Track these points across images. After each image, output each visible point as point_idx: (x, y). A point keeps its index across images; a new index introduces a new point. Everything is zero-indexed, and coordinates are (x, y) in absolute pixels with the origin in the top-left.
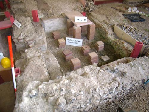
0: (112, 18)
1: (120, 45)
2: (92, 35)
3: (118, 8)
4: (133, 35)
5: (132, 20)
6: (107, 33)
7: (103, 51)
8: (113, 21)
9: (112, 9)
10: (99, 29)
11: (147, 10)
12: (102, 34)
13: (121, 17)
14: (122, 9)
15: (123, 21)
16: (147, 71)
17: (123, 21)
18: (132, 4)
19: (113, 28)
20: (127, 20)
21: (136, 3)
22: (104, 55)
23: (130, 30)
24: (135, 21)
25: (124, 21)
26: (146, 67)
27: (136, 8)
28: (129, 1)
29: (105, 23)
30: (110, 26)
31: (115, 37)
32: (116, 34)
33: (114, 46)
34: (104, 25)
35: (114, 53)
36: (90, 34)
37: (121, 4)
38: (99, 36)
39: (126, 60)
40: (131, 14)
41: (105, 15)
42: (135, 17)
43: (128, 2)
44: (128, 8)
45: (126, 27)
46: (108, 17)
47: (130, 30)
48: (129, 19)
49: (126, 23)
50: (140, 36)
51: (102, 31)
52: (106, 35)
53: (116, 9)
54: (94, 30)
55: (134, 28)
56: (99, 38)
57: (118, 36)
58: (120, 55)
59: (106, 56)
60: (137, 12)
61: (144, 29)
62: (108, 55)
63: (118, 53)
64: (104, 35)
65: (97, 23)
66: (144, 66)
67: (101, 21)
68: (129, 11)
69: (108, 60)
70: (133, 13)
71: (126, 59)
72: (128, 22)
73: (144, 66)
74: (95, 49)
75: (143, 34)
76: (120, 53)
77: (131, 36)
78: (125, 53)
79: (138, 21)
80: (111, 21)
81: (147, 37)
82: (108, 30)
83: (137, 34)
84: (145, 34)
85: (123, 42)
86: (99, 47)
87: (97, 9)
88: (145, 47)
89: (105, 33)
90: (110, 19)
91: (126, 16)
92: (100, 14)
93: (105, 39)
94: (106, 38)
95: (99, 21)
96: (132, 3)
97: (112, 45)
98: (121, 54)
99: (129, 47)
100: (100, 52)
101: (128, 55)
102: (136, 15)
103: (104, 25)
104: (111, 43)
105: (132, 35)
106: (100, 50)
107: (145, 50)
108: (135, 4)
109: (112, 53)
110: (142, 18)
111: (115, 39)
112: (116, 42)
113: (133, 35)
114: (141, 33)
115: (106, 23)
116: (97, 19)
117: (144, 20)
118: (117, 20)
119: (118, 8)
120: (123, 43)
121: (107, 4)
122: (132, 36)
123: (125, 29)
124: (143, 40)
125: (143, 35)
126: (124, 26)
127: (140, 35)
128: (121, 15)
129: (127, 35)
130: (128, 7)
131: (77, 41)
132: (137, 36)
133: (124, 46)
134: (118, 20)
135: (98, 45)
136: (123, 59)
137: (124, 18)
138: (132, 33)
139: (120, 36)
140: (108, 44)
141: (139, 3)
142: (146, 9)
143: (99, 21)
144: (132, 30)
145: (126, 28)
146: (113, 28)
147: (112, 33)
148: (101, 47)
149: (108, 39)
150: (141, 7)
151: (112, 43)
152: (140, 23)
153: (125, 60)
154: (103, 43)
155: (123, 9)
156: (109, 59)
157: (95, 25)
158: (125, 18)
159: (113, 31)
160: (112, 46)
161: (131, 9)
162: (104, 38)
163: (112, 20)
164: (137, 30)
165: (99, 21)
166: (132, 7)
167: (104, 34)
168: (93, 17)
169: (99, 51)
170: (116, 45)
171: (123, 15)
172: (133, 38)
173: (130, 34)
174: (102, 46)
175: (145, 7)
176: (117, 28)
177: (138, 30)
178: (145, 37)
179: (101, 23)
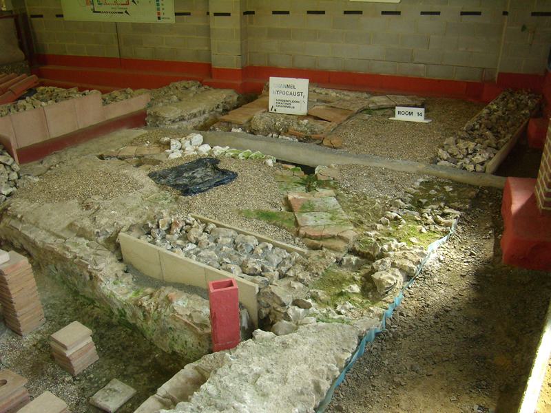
0: (107, 203)
1: (159, 313)
2: (26, 309)
3: (131, 151)
4: (202, 253)
5: (186, 191)
6: (96, 278)
7: (97, 366)
8: (112, 216)
9: (104, 165)
10: (59, 267)
11: (236, 134)
12: (80, 287)
13: (142, 186)
14: (146, 152)
15: (154, 202)
16: (279, 398)
17: (154, 202)
18: (184, 123)
19: (113, 244)
20: (170, 194)
21: (195, 116)
22: (108, 381)
23: (185, 238)
24: (200, 191)
25: (157, 204)
26: (271, 380)
27: (198, 138)
28: (166, 115)
29: (80, 236)
30: (101, 239)
31: (136, 282)
32: (138, 266)
33: (139, 324)
34: (76, 245)
35: (150, 352)
36: (16, 306)
37: (142, 132)
38: (71, 298)
39: (196, 372)
40: (181, 163)
41: (74, 197)
42: (199, 174)
43: (164, 118)
44: (168, 144)
45: (166, 228)
46: (89, 200)
47: (185, 238)
48: (176, 186)
49: (167, 209)
50: (228, 245)
51: (72, 273)
52: (93, 287)
53: (122, 159)
54: (31, 281)
55: (202, 221)
56: (70, 310)
57: (147, 273)
58: (174, 353)
59: (117, 385)
60: (205, 149)
61: (240, 212)
62: (124, 377)
63: (167, 350)
64: (88, 290)
65: (44, 243)
66: (264, 381)
67: (56, 230)
68: (175, 153)
69: (129, 400)
70: (188, 156)
71: (196, 368)
72: (176, 199)
73: (264, 381)
74: (59, 371)
75: (239, 233)
76: (171, 347)
77: (193, 261)
78: (191, 339)
79: (210, 187)
80: (103, 216)
81: (256, 242)
82: (97, 265)
83: (216, 241)
84: (246, 234)
85: (167, 297)
86: (68, 353)
87: (37, 180)
88: (257, 287)
89: (88, 278)
90: (98, 208)
91: (165, 177)
92: (52, 197)
93: (97, 304)
94: (100, 300)
95: (48, 231)
96: (182, 119)
97: (132, 322)
98: (177, 348)
99: (198, 308)
100: (84, 375)
101: (203, 343)
102: (200, 162)
103: (76, 245)
104: (123, 314)
105: (196, 253)
106: (79, 365)
107: (263, 300)
108: (193, 120)
109: (140, 358)
110: (224, 172)
111: (137, 293)
112: (141, 306)
113: (202, 253)
114: (232, 233)
115: (82, 233)
116: (41, 225)
117: (235, 175)
118: (129, 206)
119: (131, 151)
120: (169, 301)
121: (81, 147)
122: (199, 257)
123: (164, 238)
124: (244, 258)
125: (239, 238)
126: (158, 226)
127: (229, 240)
128: (144, 181)
129: (177, 259)
130: (166, 139)
131: (291, 94)
132: (217, 253)
133: (174, 311)
134: (133, 203)
135: (65, 347)
136: (185, 376)
137: (155, 188)
138: (196, 244)
139: (153, 271)
140: (114, 320)
141: (206, 115)
142: (233, 130)
143: (54, 234)
144: (193, 234)
145: (169, 231)
146: (113, 244)
147: (119, 268)
148: (83, 352)
149: (106, 300)
150: (214, 129)
151: (129, 313)
152: (219, 190)
153: (190, 375)
154: (87, 331)
155: (149, 150)
156: (131, 391)
157: (24, 261)
158: (163, 187)
159: (121, 260)
160: (134, 328)
161: (179, 145)
162: (93, 302)
163: (106, 213)
164: (211, 226)
165: (54, 234)
166: (182, 134)
167: (84, 284)
168: (20, 220)
169: (77, 370)
170: (144, 316)
171: (151, 175)
172: (204, 265)
173: (188, 254)
174: (84, 343)
175: (229, 126)
176: (133, 242)
177: (218, 226)
178: (247, 245)
179: (60, 240)
